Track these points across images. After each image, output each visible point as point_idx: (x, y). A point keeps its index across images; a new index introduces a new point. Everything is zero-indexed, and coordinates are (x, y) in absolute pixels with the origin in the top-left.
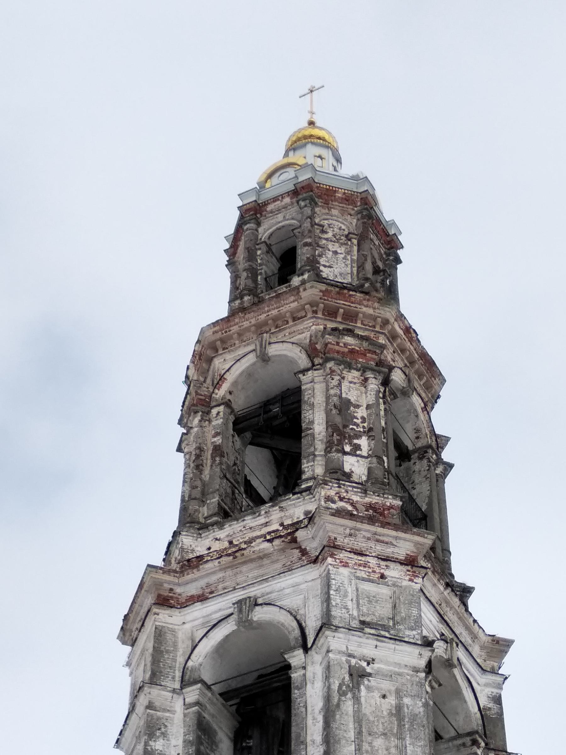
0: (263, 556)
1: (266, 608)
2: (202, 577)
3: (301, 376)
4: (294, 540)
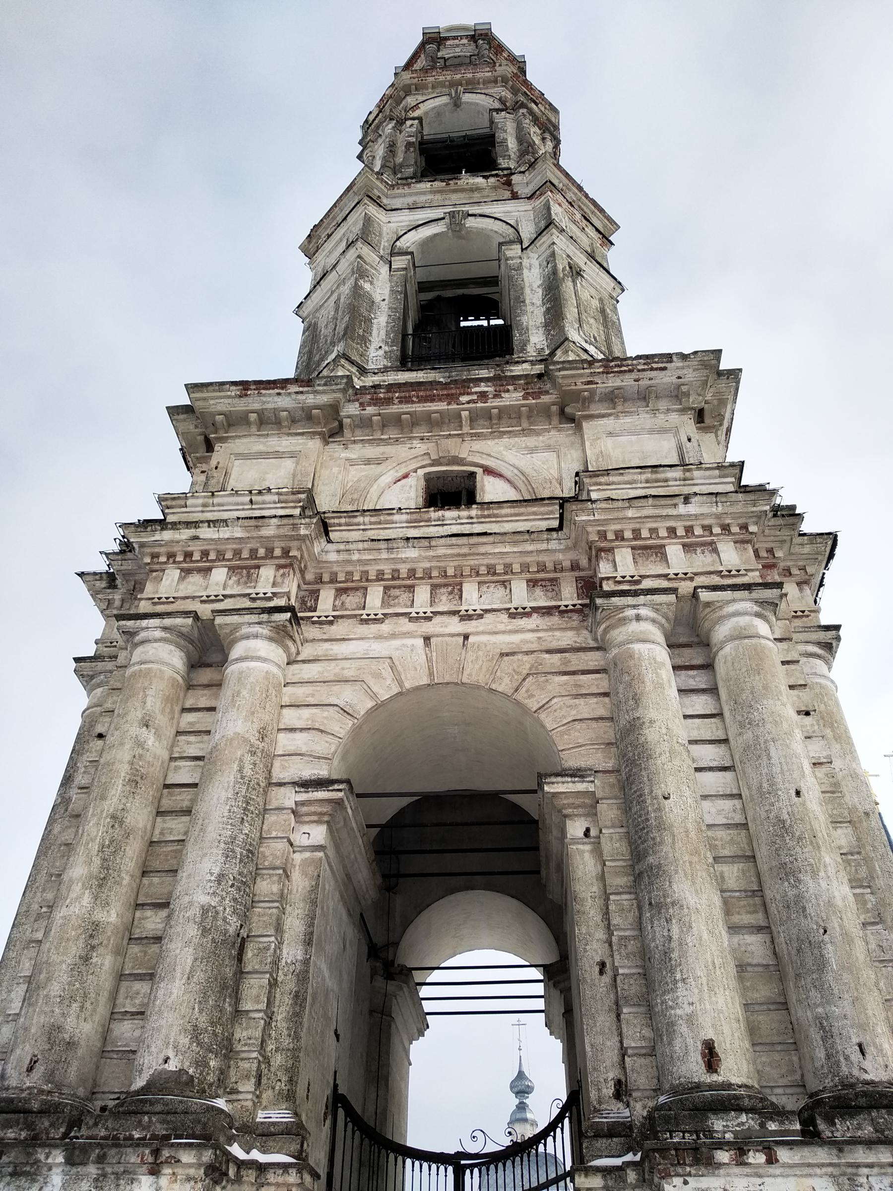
2: (411, 195)
3: (494, 113)
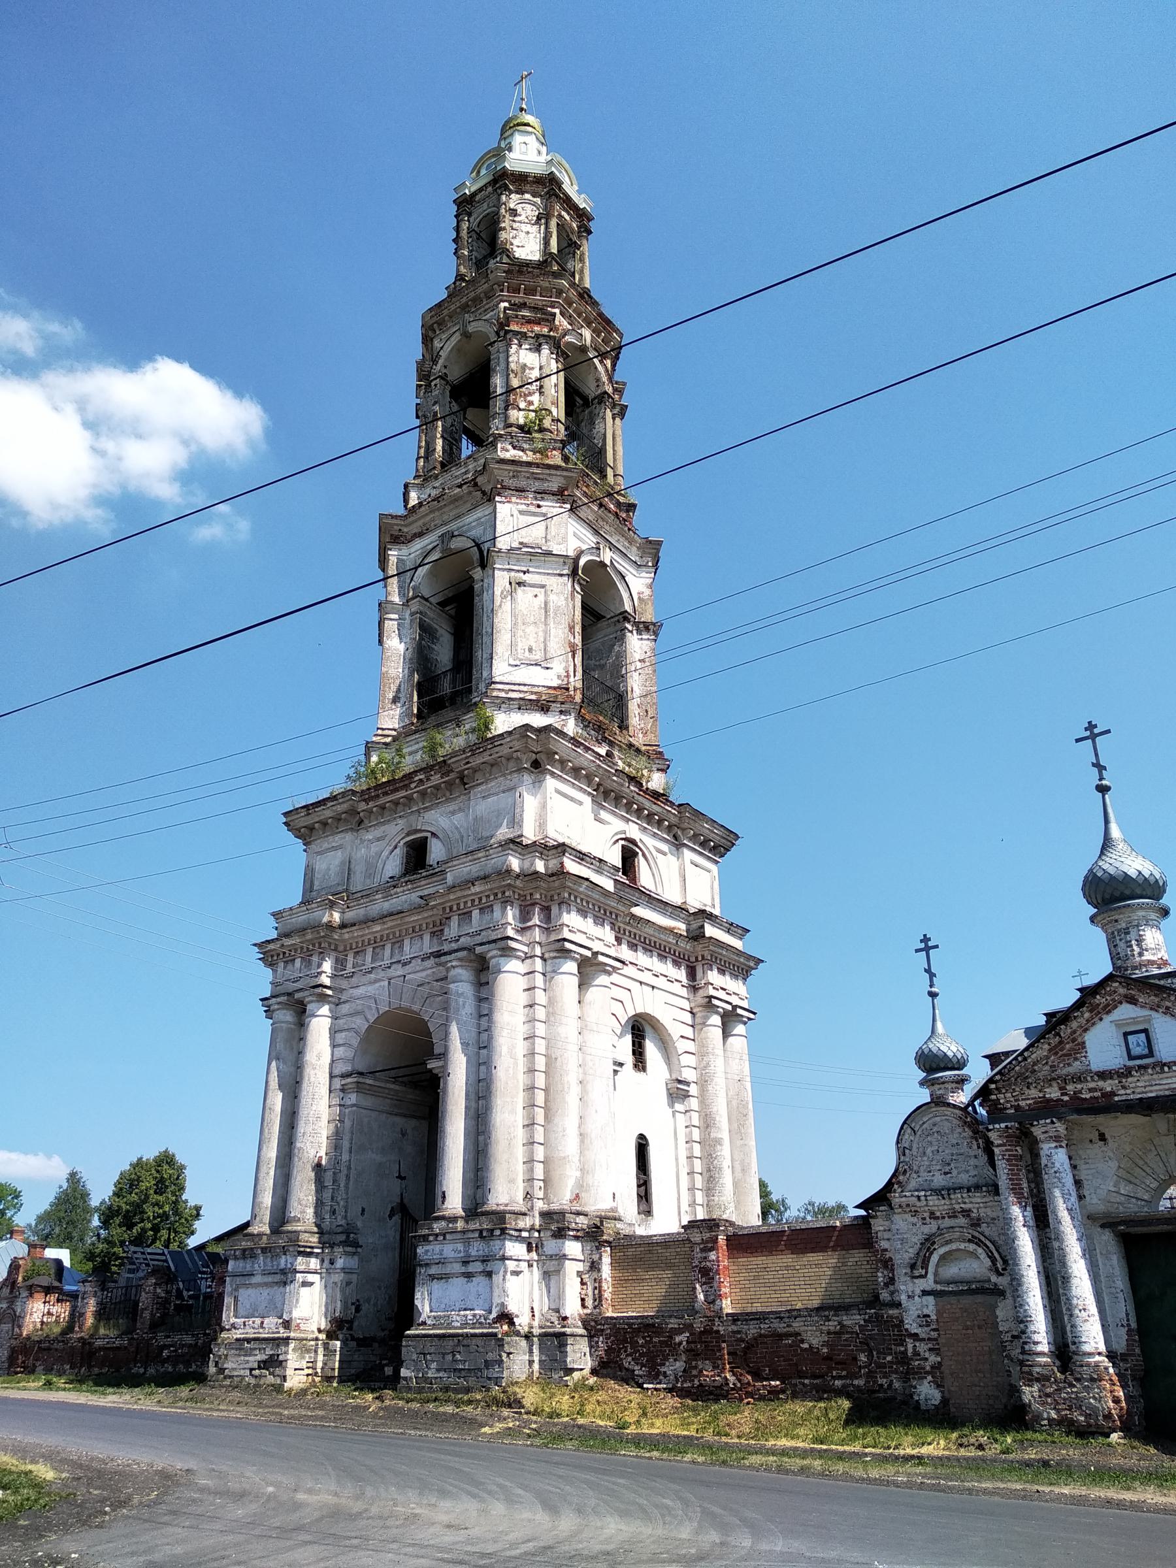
0: (456, 499)
1: (459, 538)
2: (419, 519)
4: (476, 485)
